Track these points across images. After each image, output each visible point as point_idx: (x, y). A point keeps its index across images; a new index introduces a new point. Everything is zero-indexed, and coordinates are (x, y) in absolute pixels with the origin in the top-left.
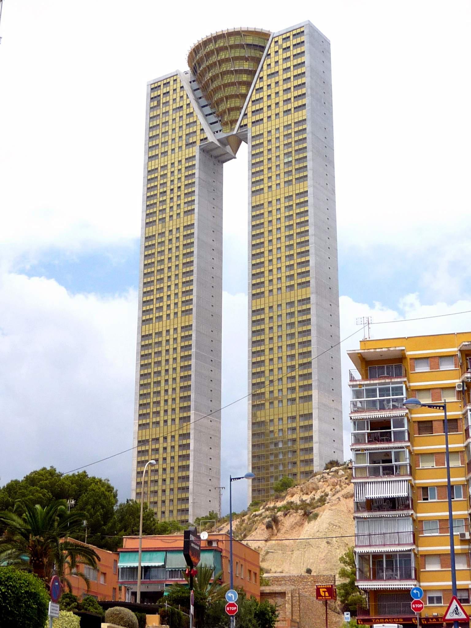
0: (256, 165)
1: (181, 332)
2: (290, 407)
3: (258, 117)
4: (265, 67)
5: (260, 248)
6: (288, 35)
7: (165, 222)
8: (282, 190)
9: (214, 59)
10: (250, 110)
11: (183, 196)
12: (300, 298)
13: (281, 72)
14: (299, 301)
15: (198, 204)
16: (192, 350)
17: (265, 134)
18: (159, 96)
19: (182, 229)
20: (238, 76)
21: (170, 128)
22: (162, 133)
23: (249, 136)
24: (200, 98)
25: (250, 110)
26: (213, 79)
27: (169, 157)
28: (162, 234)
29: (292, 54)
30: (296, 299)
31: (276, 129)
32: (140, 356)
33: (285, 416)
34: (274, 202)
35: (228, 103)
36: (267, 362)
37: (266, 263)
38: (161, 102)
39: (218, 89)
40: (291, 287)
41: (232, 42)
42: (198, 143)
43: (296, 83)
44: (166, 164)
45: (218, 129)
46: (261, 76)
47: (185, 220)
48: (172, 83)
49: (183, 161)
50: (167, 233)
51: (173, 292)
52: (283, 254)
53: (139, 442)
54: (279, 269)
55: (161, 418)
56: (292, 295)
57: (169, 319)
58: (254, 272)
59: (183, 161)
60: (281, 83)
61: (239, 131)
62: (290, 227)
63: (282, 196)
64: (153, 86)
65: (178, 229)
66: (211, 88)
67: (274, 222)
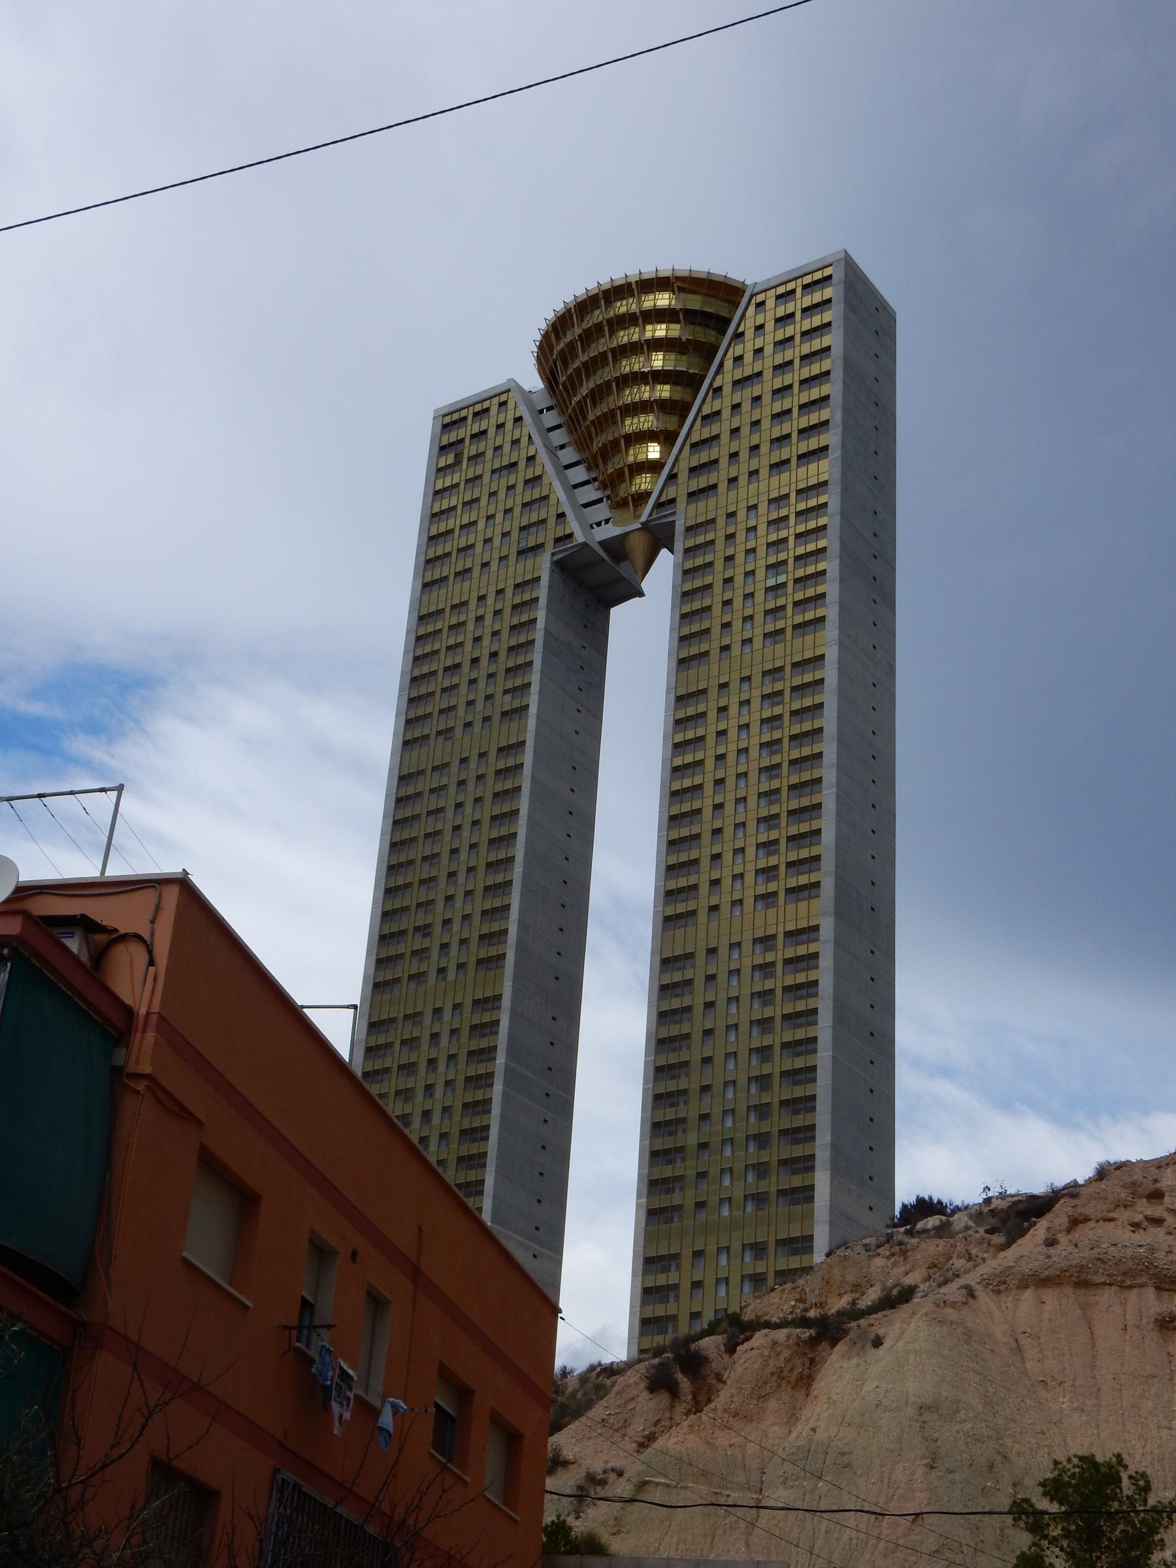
0: (691, 646)
2: (760, 915)
3: (703, 481)
4: (729, 364)
6: (791, 286)
12: (791, 927)
14: (788, 934)
18: (462, 441)
24: (562, 447)
26: (598, 394)
30: (781, 929)
31: (749, 508)
33: (748, 936)
35: (631, 452)
38: (466, 455)
39: (606, 420)
42: (550, 548)
43: (804, 423)
46: (716, 385)
48: (494, 410)
60: (767, 398)
61: (654, 516)
64: (447, 420)
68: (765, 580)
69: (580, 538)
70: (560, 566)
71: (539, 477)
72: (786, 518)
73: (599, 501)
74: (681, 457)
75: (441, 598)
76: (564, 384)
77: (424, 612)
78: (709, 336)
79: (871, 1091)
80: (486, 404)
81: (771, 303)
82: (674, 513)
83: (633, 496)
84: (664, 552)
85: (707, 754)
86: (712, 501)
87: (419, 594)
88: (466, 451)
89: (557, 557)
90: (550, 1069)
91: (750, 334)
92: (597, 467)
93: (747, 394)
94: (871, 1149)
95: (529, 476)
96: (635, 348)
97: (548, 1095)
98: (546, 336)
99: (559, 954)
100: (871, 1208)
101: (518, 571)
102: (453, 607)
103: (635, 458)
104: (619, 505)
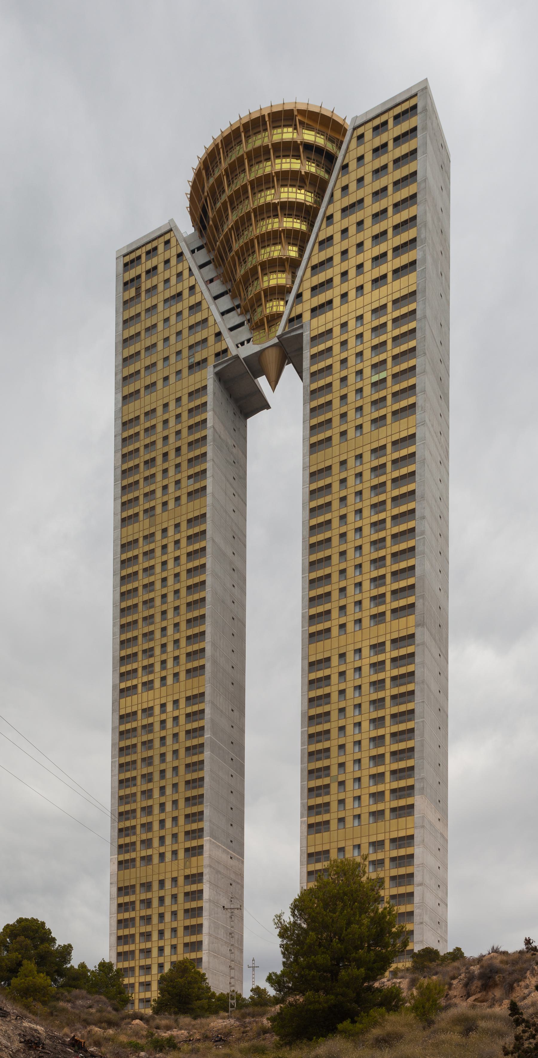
3: (322, 298)
4: (338, 194)
6: (383, 118)
10: (307, 285)
16: (205, 753)
24: (211, 281)
28: (149, 537)
32: (117, 750)
38: (143, 289)
42: (212, 361)
46: (328, 214)
48: (161, 248)
53: (120, 889)
55: (154, 852)
58: (313, 694)
60: (368, 222)
64: (127, 259)
65: (176, 702)
68: (371, 377)
70: (219, 376)
71: (199, 304)
72: (385, 325)
73: (241, 325)
75: (137, 408)
77: (126, 419)
80: (154, 244)
81: (369, 135)
82: (302, 327)
83: (267, 317)
86: (329, 314)
93: (353, 218)
96: (266, 182)
98: (198, 174)
101: (192, 381)
104: (257, 326)
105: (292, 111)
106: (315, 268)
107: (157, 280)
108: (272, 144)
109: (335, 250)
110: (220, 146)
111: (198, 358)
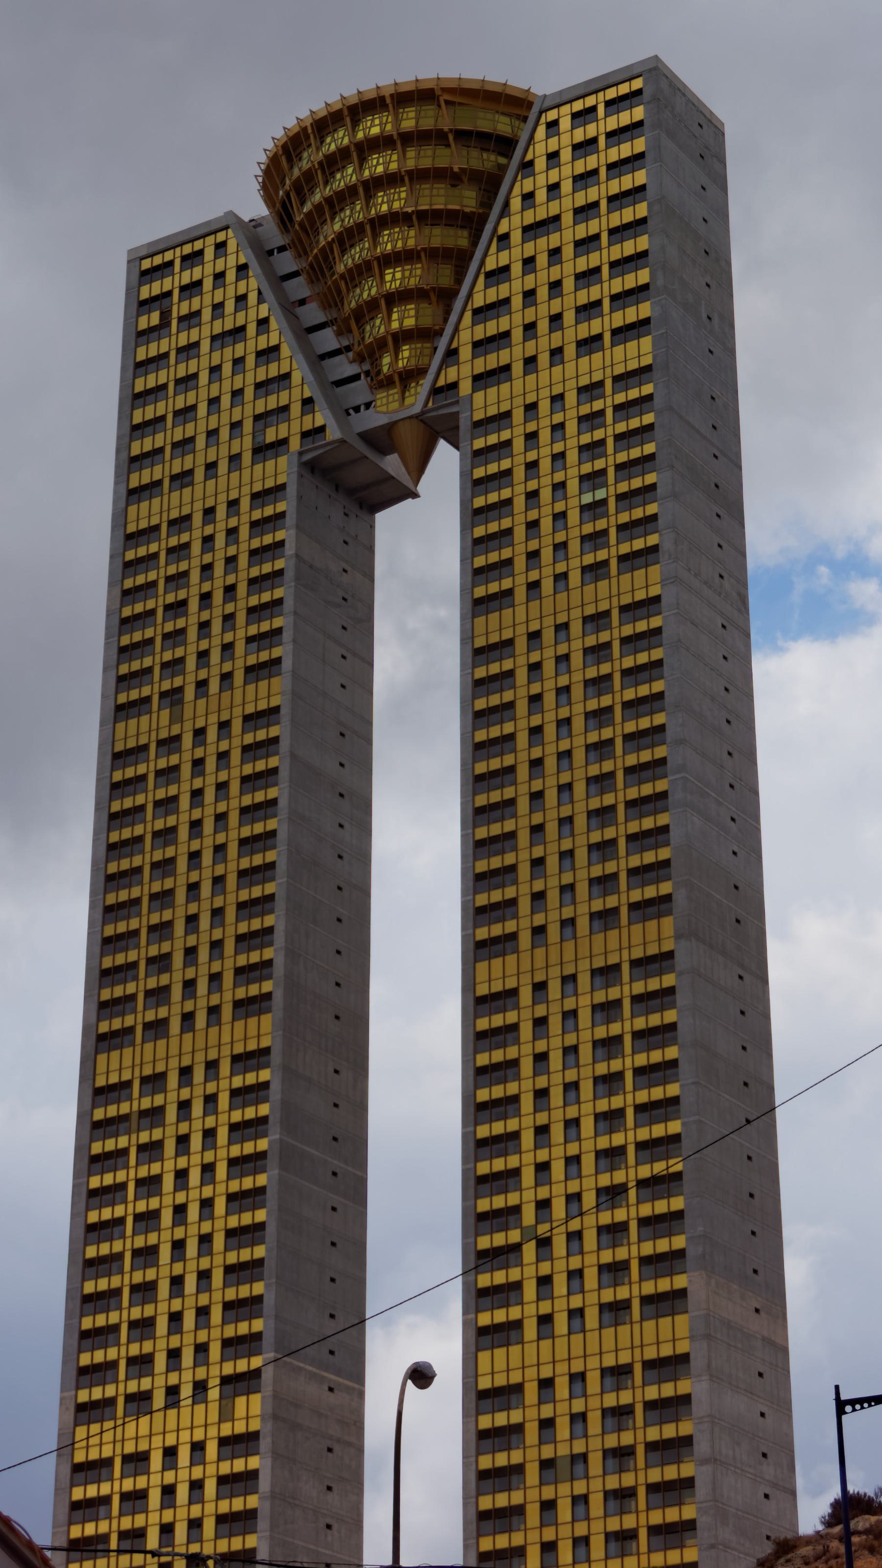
1: (235, 986)
3: (492, 361)
4: (516, 203)
5: (503, 920)
6: (590, 101)
7: (181, 702)
8: (575, 596)
9: (348, 176)
11: (241, 618)
12: (638, 953)
13: (567, 219)
14: (635, 963)
15: (294, 641)
17: (518, 415)
18: (169, 294)
19: (237, 726)
20: (427, 230)
21: (202, 427)
22: (178, 382)
23: (464, 425)
24: (302, 302)
25: (465, 336)
27: (199, 488)
28: (170, 743)
29: (604, 226)
30: (625, 956)
34: (548, 635)
35: (395, 316)
36: (524, 871)
37: (523, 805)
38: (175, 314)
39: (360, 274)
40: (615, 1311)
41: (408, 123)
42: (295, 444)
44: (186, 511)
45: (360, 400)
47: (250, 696)
48: (209, 253)
49: (245, 503)
50: (187, 740)
51: (205, 938)
52: (582, 874)
54: (567, 855)
55: (156, 1383)
56: (613, 944)
57: (192, 1029)
59: (245, 503)
62: (600, 716)
63: (576, 614)
64: (146, 264)
66: (341, 268)
67: (550, 731)
69: (333, 433)
73: (355, 378)
74: (461, 327)
76: (301, 224)
78: (488, 160)
79: (749, 1158)
82: (457, 402)
84: (443, 448)
85: (519, 725)
87: (123, 504)
88: (175, 308)
89: (307, 457)
90: (335, 1139)
91: (541, 164)
92: (350, 331)
93: (542, 244)
94: (753, 1233)
95: (263, 345)
97: (335, 1174)
99: (338, 984)
100: (757, 1311)
102: (172, 523)
103: (401, 324)
105: (432, 90)
106: (482, 313)
107: (203, 303)
108: (399, 134)
109: (514, 288)
110: (310, 131)
111: (271, 436)
